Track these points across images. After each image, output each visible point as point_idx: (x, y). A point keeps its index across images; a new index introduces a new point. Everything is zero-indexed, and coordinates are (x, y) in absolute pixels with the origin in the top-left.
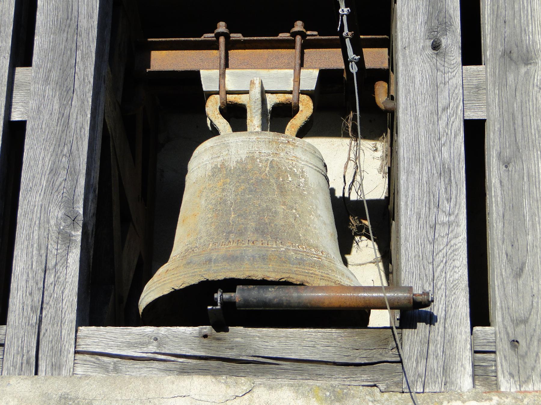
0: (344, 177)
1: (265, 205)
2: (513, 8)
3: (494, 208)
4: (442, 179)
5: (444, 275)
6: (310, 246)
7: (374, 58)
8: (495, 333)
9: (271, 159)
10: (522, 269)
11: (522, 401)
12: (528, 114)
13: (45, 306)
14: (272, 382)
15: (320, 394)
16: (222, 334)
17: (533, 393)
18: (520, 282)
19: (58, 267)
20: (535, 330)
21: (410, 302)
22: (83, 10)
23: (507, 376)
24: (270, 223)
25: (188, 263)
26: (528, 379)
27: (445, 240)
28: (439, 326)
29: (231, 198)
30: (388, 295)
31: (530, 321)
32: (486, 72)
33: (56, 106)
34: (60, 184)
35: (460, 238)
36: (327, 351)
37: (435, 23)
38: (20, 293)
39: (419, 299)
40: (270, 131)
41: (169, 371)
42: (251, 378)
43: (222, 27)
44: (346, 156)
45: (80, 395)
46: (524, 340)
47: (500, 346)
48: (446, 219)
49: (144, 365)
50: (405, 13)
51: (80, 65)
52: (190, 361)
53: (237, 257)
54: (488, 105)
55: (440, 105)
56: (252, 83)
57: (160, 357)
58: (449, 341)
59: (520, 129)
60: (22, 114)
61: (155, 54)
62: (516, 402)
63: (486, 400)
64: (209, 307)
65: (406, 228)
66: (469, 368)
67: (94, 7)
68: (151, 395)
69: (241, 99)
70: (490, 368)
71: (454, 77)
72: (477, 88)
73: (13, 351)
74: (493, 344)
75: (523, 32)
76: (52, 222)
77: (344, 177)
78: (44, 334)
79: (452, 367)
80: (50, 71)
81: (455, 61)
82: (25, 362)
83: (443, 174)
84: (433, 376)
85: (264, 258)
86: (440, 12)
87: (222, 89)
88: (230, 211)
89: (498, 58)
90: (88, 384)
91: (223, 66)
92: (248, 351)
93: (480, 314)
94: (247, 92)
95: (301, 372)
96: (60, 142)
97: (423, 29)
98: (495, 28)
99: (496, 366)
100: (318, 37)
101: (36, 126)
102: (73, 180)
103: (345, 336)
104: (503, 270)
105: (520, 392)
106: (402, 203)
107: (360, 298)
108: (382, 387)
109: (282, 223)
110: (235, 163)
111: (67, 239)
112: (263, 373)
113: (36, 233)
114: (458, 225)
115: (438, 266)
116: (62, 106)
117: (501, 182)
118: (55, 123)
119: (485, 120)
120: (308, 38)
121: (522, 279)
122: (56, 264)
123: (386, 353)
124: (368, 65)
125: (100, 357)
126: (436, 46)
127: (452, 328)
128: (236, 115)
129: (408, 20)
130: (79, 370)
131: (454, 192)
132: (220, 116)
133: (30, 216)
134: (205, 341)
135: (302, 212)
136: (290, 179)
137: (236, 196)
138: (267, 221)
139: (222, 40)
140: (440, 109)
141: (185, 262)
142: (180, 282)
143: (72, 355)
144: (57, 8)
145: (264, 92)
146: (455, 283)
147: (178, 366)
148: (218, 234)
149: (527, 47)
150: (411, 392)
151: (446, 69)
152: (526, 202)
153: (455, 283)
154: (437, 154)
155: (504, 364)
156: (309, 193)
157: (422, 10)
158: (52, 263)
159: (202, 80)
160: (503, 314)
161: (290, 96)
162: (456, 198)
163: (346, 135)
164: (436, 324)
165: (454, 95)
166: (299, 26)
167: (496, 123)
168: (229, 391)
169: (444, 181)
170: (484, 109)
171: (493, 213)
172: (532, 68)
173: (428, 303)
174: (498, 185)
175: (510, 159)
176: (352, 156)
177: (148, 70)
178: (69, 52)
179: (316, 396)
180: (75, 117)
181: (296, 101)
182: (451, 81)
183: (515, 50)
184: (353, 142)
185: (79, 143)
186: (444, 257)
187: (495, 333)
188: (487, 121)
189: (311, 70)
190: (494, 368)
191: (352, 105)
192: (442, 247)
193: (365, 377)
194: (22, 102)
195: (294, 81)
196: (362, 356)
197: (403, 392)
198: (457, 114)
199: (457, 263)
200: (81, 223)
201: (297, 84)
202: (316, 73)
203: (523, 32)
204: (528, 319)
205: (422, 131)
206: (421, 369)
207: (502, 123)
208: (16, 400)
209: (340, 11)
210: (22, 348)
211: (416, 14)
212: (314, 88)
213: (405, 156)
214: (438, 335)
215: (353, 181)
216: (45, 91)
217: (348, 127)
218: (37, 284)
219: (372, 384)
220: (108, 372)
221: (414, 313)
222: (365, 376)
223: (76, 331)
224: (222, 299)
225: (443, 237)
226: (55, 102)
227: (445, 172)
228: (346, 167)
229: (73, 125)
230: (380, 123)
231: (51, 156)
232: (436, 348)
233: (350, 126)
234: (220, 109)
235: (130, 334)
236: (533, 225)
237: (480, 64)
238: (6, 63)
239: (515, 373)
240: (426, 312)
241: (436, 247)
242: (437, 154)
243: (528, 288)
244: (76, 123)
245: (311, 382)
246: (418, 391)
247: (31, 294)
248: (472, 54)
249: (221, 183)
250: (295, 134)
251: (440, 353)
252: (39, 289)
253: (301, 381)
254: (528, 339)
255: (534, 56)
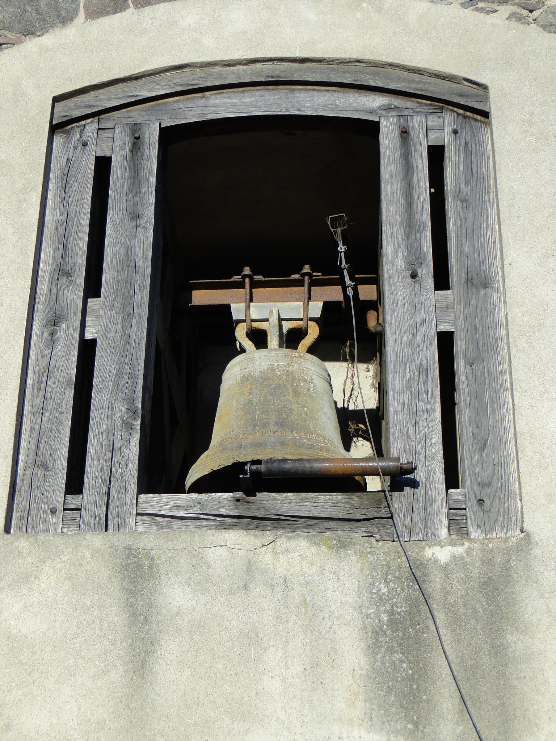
0: (344, 391)
1: (282, 405)
2: (473, 245)
3: (462, 398)
4: (421, 377)
5: (424, 450)
6: (319, 435)
7: (367, 292)
8: (465, 494)
9: (287, 369)
10: (485, 445)
11: (488, 545)
12: (487, 325)
13: (112, 479)
14: (291, 535)
15: (329, 543)
16: (251, 499)
17: (496, 540)
18: (484, 454)
19: (122, 449)
20: (496, 492)
21: (397, 470)
22: (140, 254)
23: (476, 528)
24: (287, 418)
25: (224, 450)
26: (492, 529)
27: (424, 423)
28: (421, 489)
29: (256, 399)
30: (380, 464)
31: (492, 484)
32: (453, 296)
33: (120, 327)
34: (124, 386)
35: (436, 421)
36: (334, 510)
37: (412, 258)
38: (93, 469)
39: (406, 467)
40: (286, 348)
41: (211, 527)
42: (274, 531)
43: (247, 271)
44: (345, 375)
45: (141, 546)
46: (488, 500)
47: (469, 504)
48: (424, 407)
49: (190, 523)
50: (389, 251)
51: (138, 295)
52: (226, 519)
53: (262, 444)
54: (455, 320)
55: (418, 320)
56: (271, 312)
57: (203, 516)
58: (429, 501)
59: (481, 337)
60: (94, 333)
61: (195, 293)
62: (483, 547)
63: (459, 545)
64: (241, 476)
65: (394, 415)
66: (445, 522)
67: (148, 248)
68: (196, 545)
69: (263, 326)
70: (462, 521)
71: (429, 298)
72: (446, 307)
73: (88, 514)
74: (463, 503)
75: (482, 264)
76: (118, 415)
77: (344, 391)
78: (112, 500)
79: (432, 521)
80: (114, 300)
81: (429, 287)
82: (97, 522)
83: (421, 373)
84: (417, 528)
85: (283, 444)
86: (416, 250)
87: (248, 318)
88: (256, 409)
89: (462, 283)
90: (146, 537)
91: (248, 301)
92: (272, 511)
93: (452, 480)
94: (267, 320)
95: (314, 527)
96: (123, 354)
97: (403, 263)
98: (459, 261)
99: (466, 519)
100: (322, 277)
101: (104, 342)
102: (133, 382)
103: (348, 498)
104: (471, 446)
105: (486, 538)
106: (390, 395)
107: (359, 466)
108: (377, 537)
109: (296, 418)
110: (259, 373)
111: (129, 427)
112: (284, 528)
113: (105, 423)
114: (434, 412)
115: (420, 443)
116: (125, 326)
117: (467, 378)
118: (119, 340)
119: (453, 332)
120: (314, 278)
121: (485, 452)
122: (121, 447)
123: (380, 511)
124: (362, 298)
125: (156, 518)
126: (414, 276)
127: (431, 491)
128: (259, 338)
129: (392, 256)
130: (140, 528)
131: (431, 387)
132: (247, 339)
133: (100, 410)
134: (238, 504)
135: (312, 410)
136: (302, 385)
137: (260, 397)
138: (285, 416)
139: (247, 280)
140: (418, 324)
141: (221, 449)
142: (217, 464)
143: (134, 516)
144: (119, 253)
145: (280, 320)
146: (432, 456)
147: (217, 524)
148: (247, 427)
149: (485, 275)
150: (400, 541)
151: (422, 293)
152: (487, 393)
153: (432, 456)
154: (416, 358)
155: (473, 517)
156: (317, 396)
157: (402, 248)
158: (117, 446)
159: (232, 311)
160: (471, 479)
161: (301, 323)
162: (432, 391)
163: (345, 360)
164: (419, 488)
165: (429, 312)
166: (307, 269)
167: (462, 333)
168: (257, 541)
169: (423, 378)
170: (453, 324)
171: (461, 402)
172: (489, 291)
173: (412, 470)
174: (465, 380)
175: (474, 360)
176: (350, 375)
177: (190, 305)
178: (129, 286)
179: (326, 544)
180: (134, 334)
181: (305, 326)
182: (426, 301)
183: (475, 277)
184: (350, 365)
185: (138, 354)
186: (423, 436)
187: (465, 494)
188: (455, 332)
189: (317, 302)
190: (465, 521)
191: (349, 334)
192: (422, 429)
193: (363, 530)
194: (93, 324)
195: (304, 311)
196: (361, 513)
197: (394, 541)
198: (431, 327)
199: (434, 441)
200: (140, 415)
201: (306, 313)
202: (321, 304)
203: (482, 264)
204: (491, 483)
205: (405, 340)
206: (408, 523)
207: (466, 333)
208: (90, 551)
209: (339, 249)
210: (95, 512)
211: (398, 252)
212: (319, 316)
213: (392, 359)
214: (420, 497)
215: (351, 395)
216: (111, 315)
217: (346, 352)
218: (106, 462)
219: (369, 535)
220: (162, 529)
221: (401, 479)
222: (364, 528)
223: (137, 498)
224: (250, 470)
225: (423, 421)
226: (119, 324)
227: (423, 371)
228: (345, 384)
229: (133, 340)
230: (370, 347)
231: (116, 364)
232: (419, 506)
233: (347, 351)
234: (247, 333)
235: (179, 499)
236: (493, 411)
237: (449, 289)
238: (80, 294)
239: (482, 525)
240: (411, 479)
241: (417, 429)
242: (416, 358)
243: (491, 459)
244: (136, 339)
245: (321, 534)
246: (406, 540)
247: (101, 470)
248: (442, 281)
249: (248, 388)
250: (306, 351)
251: (422, 510)
252: (108, 466)
253: (314, 533)
254: (492, 498)
255: (490, 282)
